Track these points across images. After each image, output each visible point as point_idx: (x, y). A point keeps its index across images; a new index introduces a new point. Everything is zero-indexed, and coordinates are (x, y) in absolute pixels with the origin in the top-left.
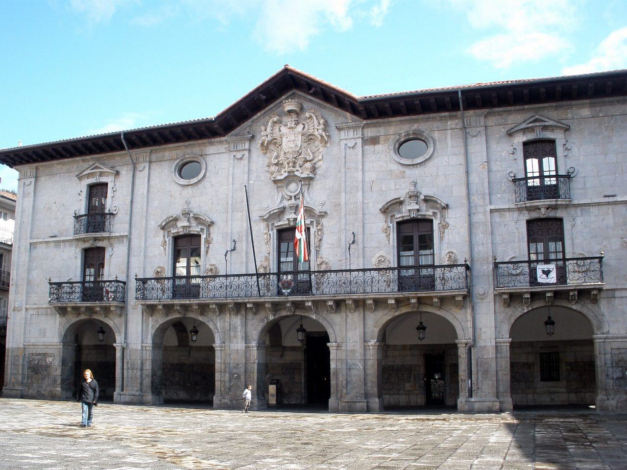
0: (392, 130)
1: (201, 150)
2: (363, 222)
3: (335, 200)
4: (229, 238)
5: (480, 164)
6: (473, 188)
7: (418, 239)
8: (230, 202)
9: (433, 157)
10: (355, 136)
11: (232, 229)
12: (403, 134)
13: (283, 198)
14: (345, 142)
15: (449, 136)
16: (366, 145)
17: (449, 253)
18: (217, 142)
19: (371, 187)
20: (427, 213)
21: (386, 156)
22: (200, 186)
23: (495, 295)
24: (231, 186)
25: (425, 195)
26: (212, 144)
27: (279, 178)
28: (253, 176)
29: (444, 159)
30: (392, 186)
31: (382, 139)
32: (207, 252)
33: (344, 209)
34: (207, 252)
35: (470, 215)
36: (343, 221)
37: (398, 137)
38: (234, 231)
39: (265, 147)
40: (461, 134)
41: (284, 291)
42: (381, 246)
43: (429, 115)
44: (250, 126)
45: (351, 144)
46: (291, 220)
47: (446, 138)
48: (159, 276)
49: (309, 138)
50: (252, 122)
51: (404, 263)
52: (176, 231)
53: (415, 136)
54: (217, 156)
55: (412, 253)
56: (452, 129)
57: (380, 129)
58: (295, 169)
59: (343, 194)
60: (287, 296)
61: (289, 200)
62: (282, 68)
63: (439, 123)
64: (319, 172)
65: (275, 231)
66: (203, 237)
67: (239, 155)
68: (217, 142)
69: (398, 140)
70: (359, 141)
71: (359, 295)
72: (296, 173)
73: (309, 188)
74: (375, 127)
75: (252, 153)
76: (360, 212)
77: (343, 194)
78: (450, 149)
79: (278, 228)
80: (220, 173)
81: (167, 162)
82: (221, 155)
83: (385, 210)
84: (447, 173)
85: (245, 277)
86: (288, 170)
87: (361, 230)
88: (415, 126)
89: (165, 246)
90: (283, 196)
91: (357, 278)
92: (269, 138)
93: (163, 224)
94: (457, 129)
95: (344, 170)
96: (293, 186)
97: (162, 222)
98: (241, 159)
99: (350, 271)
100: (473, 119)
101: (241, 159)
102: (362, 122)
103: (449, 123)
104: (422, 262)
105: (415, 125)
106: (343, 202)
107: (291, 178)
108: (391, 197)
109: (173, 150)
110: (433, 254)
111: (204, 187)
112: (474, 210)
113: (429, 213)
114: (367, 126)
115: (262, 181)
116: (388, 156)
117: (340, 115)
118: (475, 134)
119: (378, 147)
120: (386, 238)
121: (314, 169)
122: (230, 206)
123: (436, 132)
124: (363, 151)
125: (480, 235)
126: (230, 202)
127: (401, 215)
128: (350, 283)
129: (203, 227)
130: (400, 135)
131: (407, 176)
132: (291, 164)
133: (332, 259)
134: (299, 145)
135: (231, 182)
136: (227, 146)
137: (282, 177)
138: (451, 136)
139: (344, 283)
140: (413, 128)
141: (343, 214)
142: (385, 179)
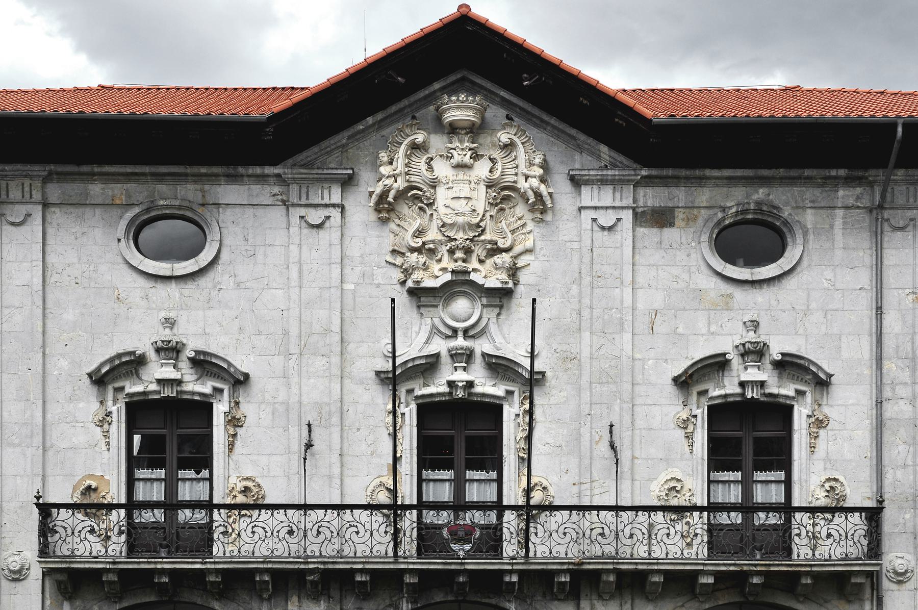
0: (704, 196)
1: (202, 191)
2: (632, 401)
3: (565, 347)
4: (294, 416)
5: (907, 291)
6: (889, 343)
7: (463, 444)
8: (294, 331)
9: (799, 269)
10: (618, 204)
11: (300, 395)
12: (734, 210)
13: (435, 331)
14: (592, 214)
15: (838, 223)
16: (641, 226)
17: (829, 480)
18: (249, 176)
19: (652, 323)
20: (783, 392)
21: (688, 255)
22: (204, 282)
23: (44, 574)
24: (294, 292)
25: (785, 351)
26: (234, 178)
27: (429, 283)
28: (353, 275)
29: (825, 273)
30: (702, 326)
31: (680, 215)
32: (231, 447)
33: (589, 371)
34: (231, 447)
35: (879, 403)
36: (586, 396)
37: (720, 215)
38: (305, 399)
39: (385, 208)
40: (868, 221)
41: (455, 547)
42: (672, 458)
43: (802, 171)
44: (343, 146)
45: (607, 219)
46: (460, 384)
47: (832, 227)
48: (94, 498)
49: (503, 194)
50: (349, 137)
51: (142, 492)
52: (139, 388)
53: (760, 217)
54: (250, 211)
55: (161, 473)
56: (847, 208)
57: (675, 191)
58: (470, 267)
59: (586, 335)
60: (463, 559)
61: (448, 337)
62: (449, 10)
63: (817, 192)
64: (523, 277)
65: (413, 406)
66: (220, 409)
67: (315, 216)
68: (249, 176)
69: (719, 222)
70: (628, 216)
71: (636, 564)
72: (474, 277)
73: (499, 314)
74: (666, 185)
75: (348, 213)
76: (627, 378)
77: (586, 335)
78: (839, 253)
79: (420, 401)
80: (260, 257)
81: (98, 211)
82: (260, 211)
83: (684, 382)
84: (831, 307)
85: (222, 510)
86: (451, 266)
87: (627, 418)
88: (761, 193)
89: (106, 426)
90: (434, 326)
91: (319, 524)
92: (401, 184)
93: (104, 370)
94: (858, 207)
95: (589, 279)
96: (461, 305)
97: (103, 364)
98: (319, 226)
99: (306, 507)
100: (900, 188)
101: (319, 226)
102: (638, 172)
103: (841, 193)
104: (428, 495)
105: (761, 191)
106: (586, 353)
107: (460, 285)
108: (701, 351)
109: (118, 182)
110: (210, 479)
111: (215, 287)
112: (887, 393)
113: (788, 390)
114: (647, 181)
115: (378, 285)
116: (693, 256)
117: (580, 149)
118: (901, 224)
119: (670, 234)
120: (685, 442)
121: (513, 271)
122: (294, 340)
123: (809, 211)
124: (634, 236)
125: (900, 448)
126: (294, 331)
127: (722, 392)
128: (617, 537)
129: (219, 385)
130: (723, 209)
131: (736, 306)
132: (459, 254)
133: (554, 479)
134: (481, 211)
135: (294, 283)
136: (276, 189)
137: (437, 283)
138: (844, 223)
139: (602, 535)
140: (755, 197)
141: (585, 378)
142: (684, 309)
